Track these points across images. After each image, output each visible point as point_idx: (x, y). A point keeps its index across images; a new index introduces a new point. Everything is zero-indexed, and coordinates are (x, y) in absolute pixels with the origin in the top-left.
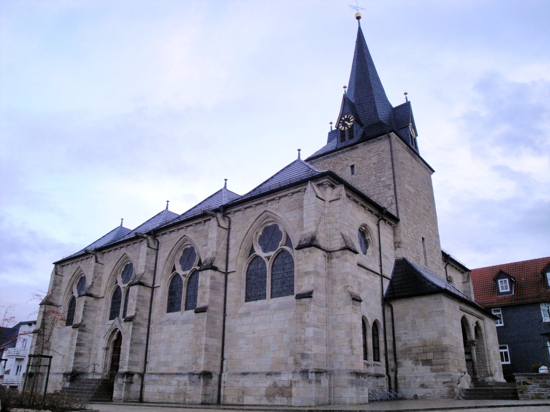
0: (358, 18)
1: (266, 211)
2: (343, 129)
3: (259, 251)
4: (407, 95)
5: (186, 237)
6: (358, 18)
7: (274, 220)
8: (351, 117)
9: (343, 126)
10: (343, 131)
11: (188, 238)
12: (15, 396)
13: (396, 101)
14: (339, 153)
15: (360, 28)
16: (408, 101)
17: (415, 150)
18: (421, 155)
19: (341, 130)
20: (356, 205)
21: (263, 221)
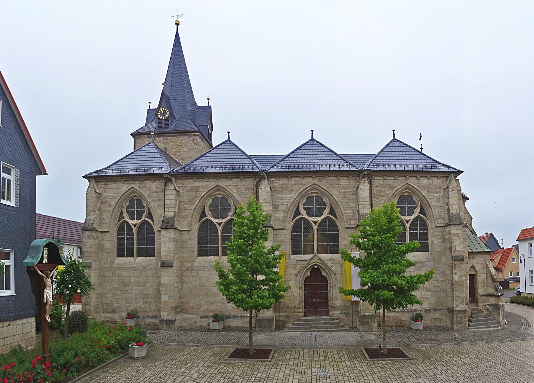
0: (177, 24)
1: (314, 184)
2: (161, 118)
3: (304, 214)
4: (209, 101)
5: (134, 189)
6: (177, 24)
7: (318, 192)
8: (168, 110)
9: (161, 116)
10: (161, 119)
11: (135, 190)
12: (209, 307)
13: (201, 102)
14: (169, 136)
15: (177, 33)
16: (210, 105)
17: (210, 143)
18: (287, 154)
19: (159, 118)
20: (204, 181)
21: (419, 198)
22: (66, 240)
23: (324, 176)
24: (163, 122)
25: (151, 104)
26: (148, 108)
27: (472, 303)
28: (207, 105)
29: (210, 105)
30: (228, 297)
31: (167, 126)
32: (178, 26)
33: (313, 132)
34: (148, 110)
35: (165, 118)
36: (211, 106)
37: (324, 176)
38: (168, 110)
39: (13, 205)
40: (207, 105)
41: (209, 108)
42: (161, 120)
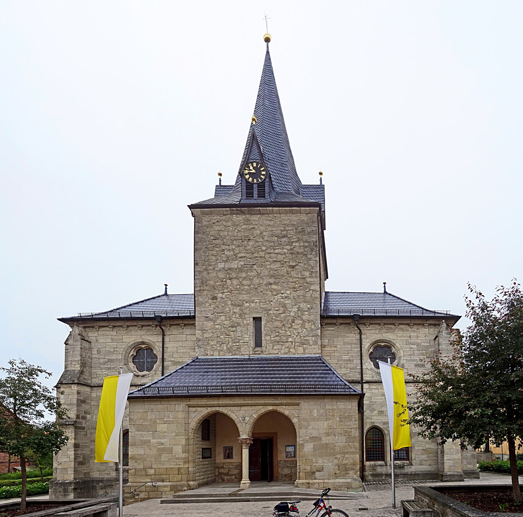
0: (267, 40)
6: (267, 40)
8: (263, 169)
19: (246, 180)
22: (315, 388)
23: (423, 324)
24: (255, 186)
25: (222, 178)
26: (218, 184)
27: (272, 473)
28: (319, 184)
29: (323, 184)
30: (69, 433)
31: (262, 195)
32: (269, 44)
33: (386, 285)
34: (217, 186)
35: (258, 181)
36: (324, 185)
37: (423, 324)
38: (263, 169)
39: (406, 445)
40: (319, 184)
41: (320, 189)
42: (252, 184)
